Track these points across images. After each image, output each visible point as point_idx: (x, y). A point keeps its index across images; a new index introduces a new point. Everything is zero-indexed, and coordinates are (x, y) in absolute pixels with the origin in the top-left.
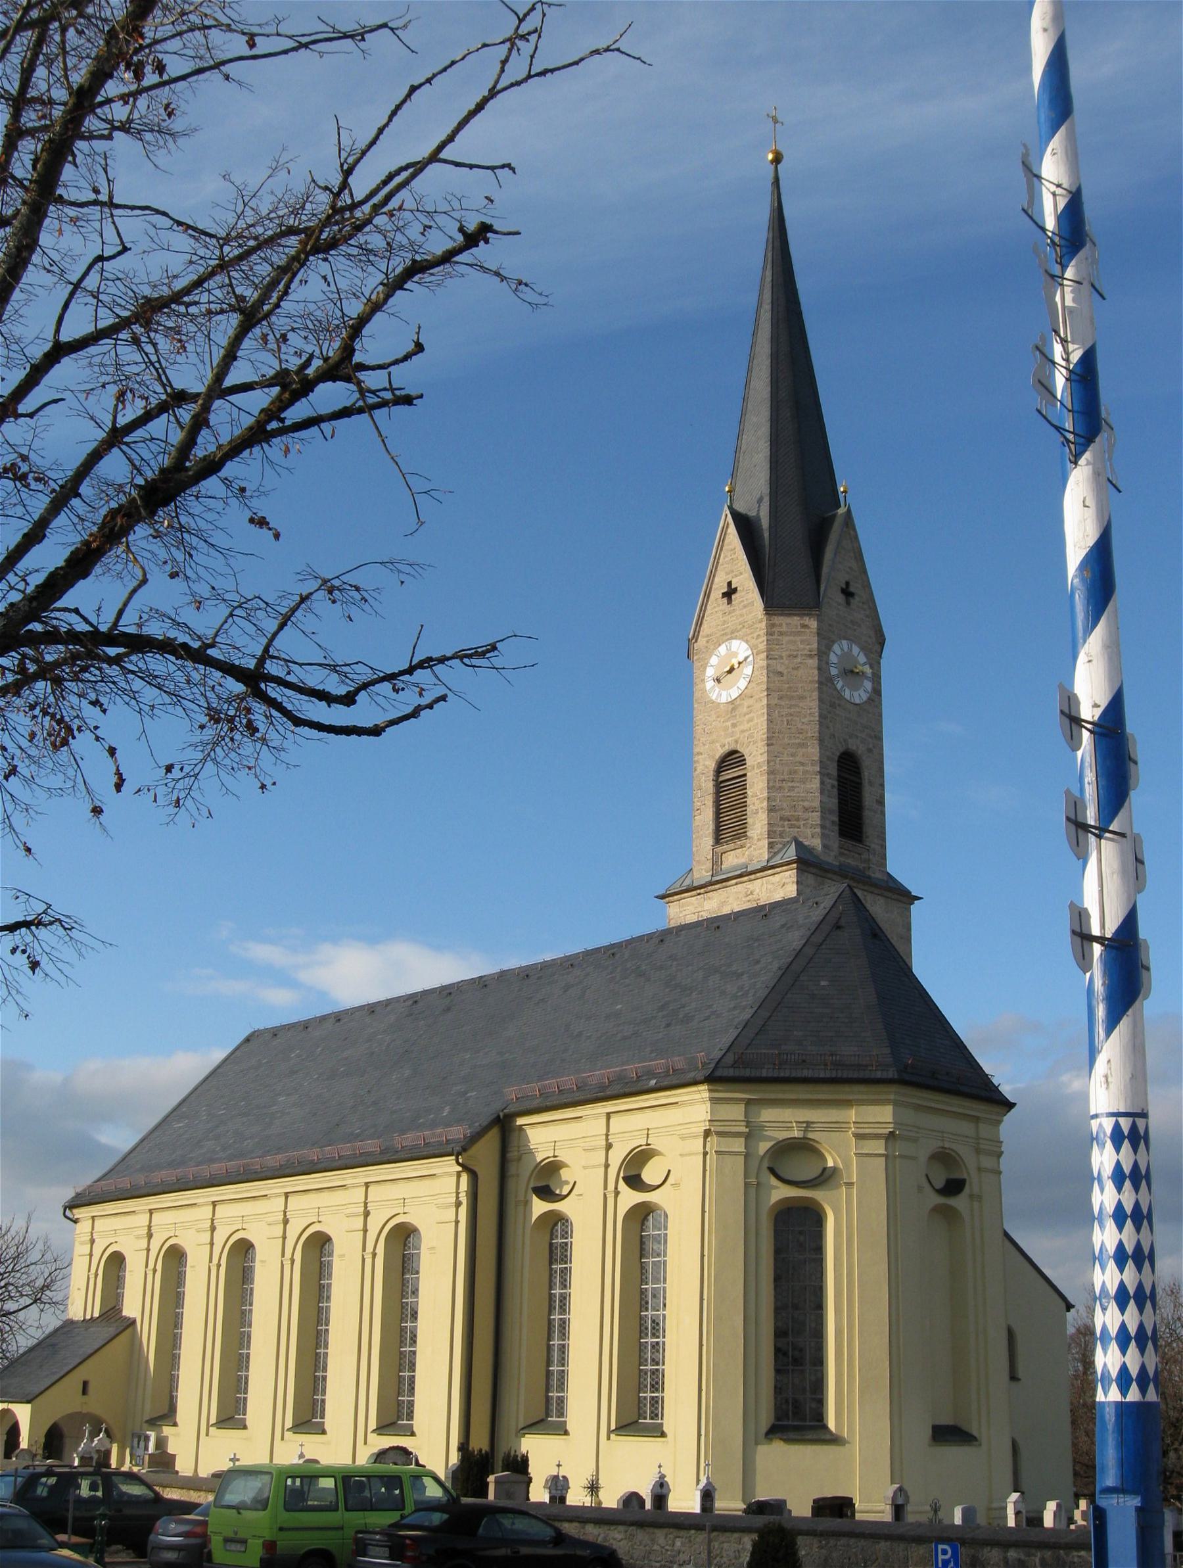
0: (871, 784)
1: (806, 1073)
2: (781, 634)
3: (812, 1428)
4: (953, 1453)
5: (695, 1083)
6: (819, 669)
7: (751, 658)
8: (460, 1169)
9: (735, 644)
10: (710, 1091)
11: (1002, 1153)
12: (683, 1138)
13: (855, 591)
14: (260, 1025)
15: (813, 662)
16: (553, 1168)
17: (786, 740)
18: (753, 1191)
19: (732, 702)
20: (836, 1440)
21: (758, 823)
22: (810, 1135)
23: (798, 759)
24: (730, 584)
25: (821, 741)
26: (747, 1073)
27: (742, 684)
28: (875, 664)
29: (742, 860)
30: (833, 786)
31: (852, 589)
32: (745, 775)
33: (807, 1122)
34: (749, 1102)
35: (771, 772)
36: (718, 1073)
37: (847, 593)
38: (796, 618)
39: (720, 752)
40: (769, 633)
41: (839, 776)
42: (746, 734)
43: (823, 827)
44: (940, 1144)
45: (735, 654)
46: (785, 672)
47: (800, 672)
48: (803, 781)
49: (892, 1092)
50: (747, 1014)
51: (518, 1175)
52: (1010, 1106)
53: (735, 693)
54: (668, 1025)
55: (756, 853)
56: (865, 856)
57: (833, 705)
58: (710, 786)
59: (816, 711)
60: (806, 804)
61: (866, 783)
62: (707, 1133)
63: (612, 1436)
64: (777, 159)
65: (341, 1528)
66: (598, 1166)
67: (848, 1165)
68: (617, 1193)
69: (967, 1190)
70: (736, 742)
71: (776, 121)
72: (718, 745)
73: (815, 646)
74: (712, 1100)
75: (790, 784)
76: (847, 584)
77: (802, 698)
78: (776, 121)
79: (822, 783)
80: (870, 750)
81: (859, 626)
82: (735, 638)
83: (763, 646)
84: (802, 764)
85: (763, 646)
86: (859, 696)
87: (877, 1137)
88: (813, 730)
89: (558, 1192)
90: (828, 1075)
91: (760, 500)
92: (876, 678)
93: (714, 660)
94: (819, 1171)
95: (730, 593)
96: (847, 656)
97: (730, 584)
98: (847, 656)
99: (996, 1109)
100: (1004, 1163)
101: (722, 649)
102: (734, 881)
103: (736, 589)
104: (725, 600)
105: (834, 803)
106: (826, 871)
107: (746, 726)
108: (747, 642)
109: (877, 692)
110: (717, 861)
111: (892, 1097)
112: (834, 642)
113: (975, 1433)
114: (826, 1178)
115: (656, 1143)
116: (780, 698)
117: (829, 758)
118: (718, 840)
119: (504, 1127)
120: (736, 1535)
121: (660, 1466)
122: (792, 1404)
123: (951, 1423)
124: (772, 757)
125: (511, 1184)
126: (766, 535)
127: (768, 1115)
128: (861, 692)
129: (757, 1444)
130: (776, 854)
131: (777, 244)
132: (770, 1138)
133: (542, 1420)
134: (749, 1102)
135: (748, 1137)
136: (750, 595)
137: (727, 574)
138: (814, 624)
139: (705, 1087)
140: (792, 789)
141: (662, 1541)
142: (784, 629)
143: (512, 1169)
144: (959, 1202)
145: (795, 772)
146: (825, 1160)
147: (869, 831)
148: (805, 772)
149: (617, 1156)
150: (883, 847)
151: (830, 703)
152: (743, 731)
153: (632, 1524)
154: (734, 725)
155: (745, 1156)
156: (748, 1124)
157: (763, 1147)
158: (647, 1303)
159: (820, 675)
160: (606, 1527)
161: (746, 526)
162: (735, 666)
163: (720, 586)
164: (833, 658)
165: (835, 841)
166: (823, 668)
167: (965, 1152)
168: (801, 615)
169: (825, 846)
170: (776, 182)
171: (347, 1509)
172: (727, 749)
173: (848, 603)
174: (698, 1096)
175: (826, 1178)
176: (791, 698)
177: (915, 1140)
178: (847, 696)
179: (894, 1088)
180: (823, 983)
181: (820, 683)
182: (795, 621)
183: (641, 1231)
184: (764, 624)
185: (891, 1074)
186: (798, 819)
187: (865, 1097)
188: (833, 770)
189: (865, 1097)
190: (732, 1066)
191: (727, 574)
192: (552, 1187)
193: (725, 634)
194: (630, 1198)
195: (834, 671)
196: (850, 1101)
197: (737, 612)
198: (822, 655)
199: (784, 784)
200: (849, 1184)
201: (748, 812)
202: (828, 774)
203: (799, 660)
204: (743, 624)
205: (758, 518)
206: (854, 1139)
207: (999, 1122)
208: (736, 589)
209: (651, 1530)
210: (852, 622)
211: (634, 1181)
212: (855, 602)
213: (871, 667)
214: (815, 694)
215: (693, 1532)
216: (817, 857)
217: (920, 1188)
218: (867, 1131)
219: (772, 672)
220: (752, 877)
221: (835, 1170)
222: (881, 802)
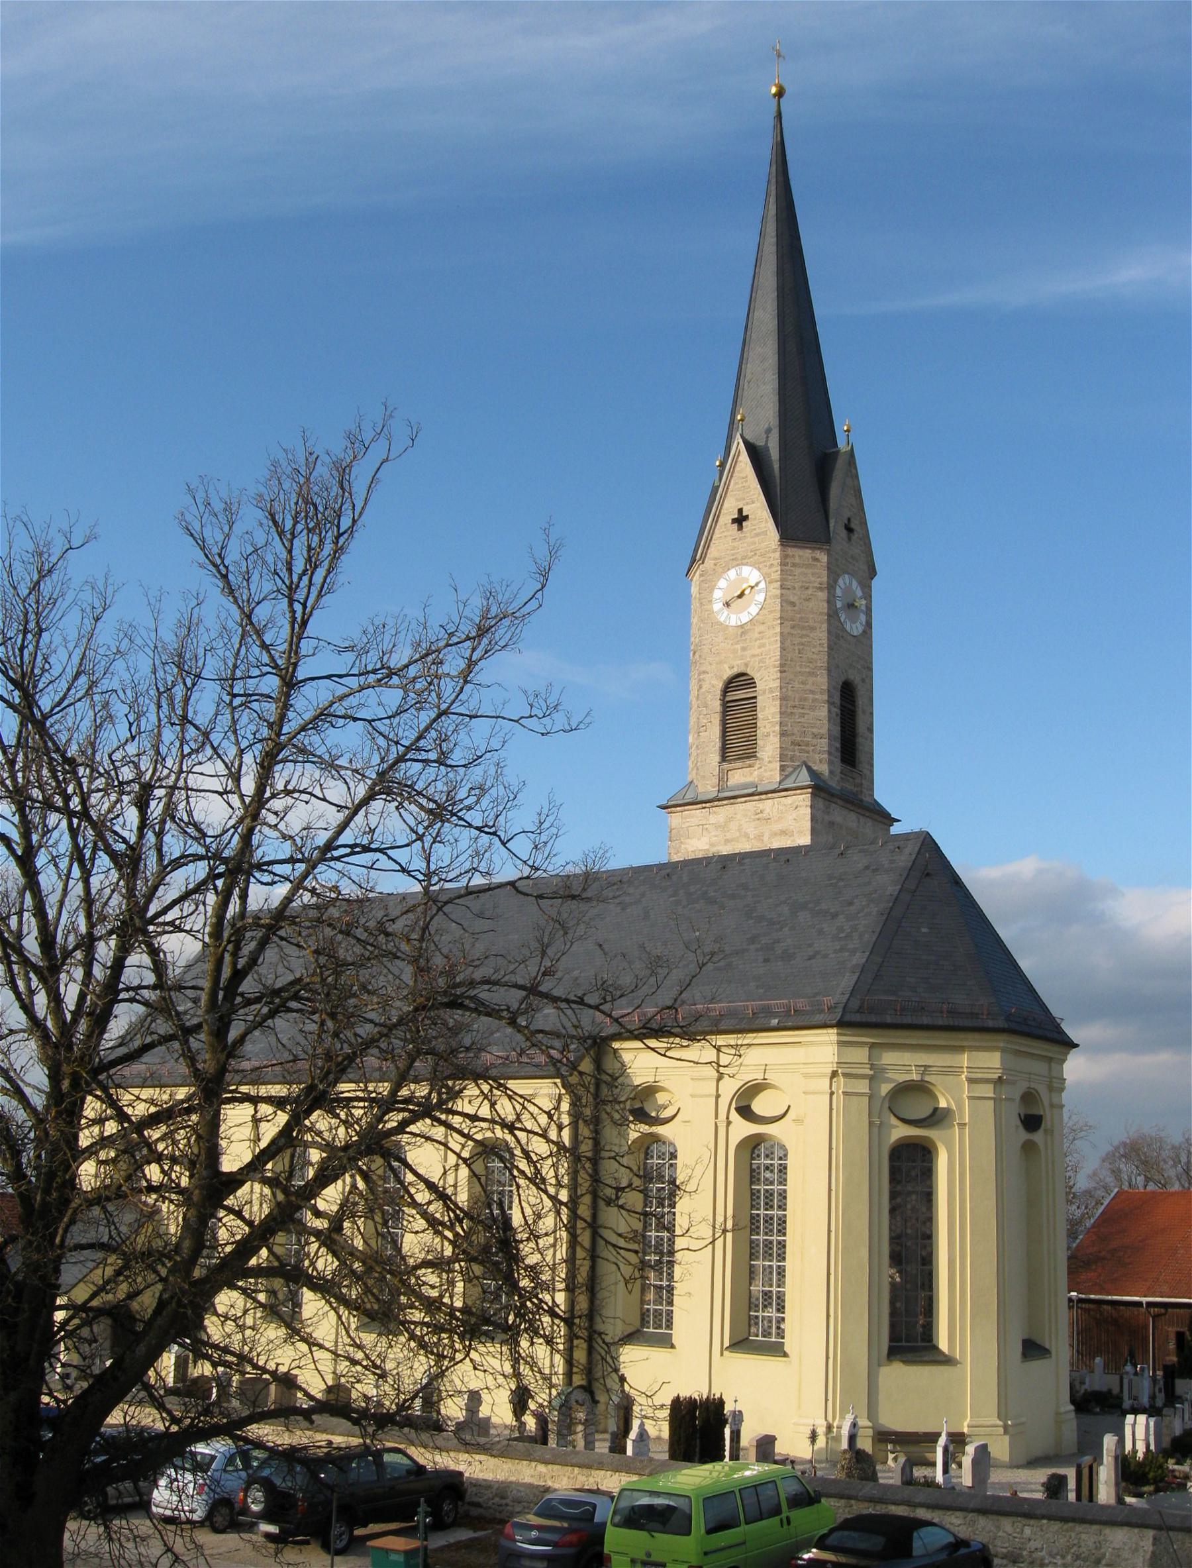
0: (864, 712)
1: (926, 1020)
2: (794, 565)
3: (926, 1349)
5: (831, 1026)
6: (828, 602)
7: (762, 585)
9: (746, 570)
10: (838, 1034)
12: (806, 1076)
13: (855, 528)
15: (823, 595)
16: (650, 1091)
17: (798, 669)
18: (875, 1130)
19: (742, 626)
20: (948, 1361)
21: (769, 745)
22: (927, 1078)
23: (808, 687)
24: (740, 511)
25: (829, 671)
26: (873, 1019)
27: (754, 610)
28: (868, 596)
29: (749, 779)
31: (853, 526)
33: (925, 1066)
34: (872, 1046)
35: (783, 698)
36: (847, 1018)
37: (849, 530)
38: (809, 551)
39: (728, 673)
40: (783, 564)
42: (757, 659)
43: (830, 753)
45: (746, 580)
46: (797, 603)
47: (811, 604)
48: (812, 708)
49: (1001, 1040)
50: (859, 959)
53: (745, 618)
55: (767, 774)
56: (858, 781)
57: (837, 637)
58: (717, 705)
59: (825, 642)
60: (815, 730)
62: (834, 1074)
63: (726, 1353)
64: (780, 94)
65: (744, 1543)
66: (710, 1096)
67: (960, 1107)
68: (729, 1123)
70: (746, 665)
72: (726, 666)
73: (825, 579)
74: (840, 1043)
76: (849, 520)
77: (813, 629)
79: (829, 711)
80: (863, 680)
82: (746, 564)
83: (777, 576)
84: (812, 692)
85: (777, 576)
86: (856, 629)
87: (987, 1081)
88: (822, 660)
89: (653, 1114)
90: (946, 1023)
91: (768, 431)
93: (722, 583)
94: (930, 1111)
95: (740, 520)
96: (848, 590)
97: (740, 511)
98: (848, 590)
101: (732, 574)
103: (747, 516)
104: (735, 526)
105: (837, 730)
106: (833, 795)
107: (758, 651)
108: (759, 569)
109: (869, 624)
110: (722, 778)
111: (1002, 1045)
112: (839, 576)
113: (1047, 1346)
114: (937, 1118)
115: (772, 1078)
116: (793, 627)
117: (834, 688)
118: (724, 758)
119: (599, 1046)
120: (1095, 1527)
122: (907, 1331)
124: (785, 684)
126: (776, 466)
127: (889, 1058)
128: (858, 624)
129: (879, 1365)
130: (787, 776)
131: (781, 178)
132: (890, 1080)
133: (638, 1331)
134: (872, 1046)
135: (872, 1079)
136: (763, 525)
137: (738, 500)
138: (824, 558)
139: (835, 1031)
140: (803, 715)
141: (1009, 1528)
142: (797, 560)
144: (1038, 1137)
145: (805, 699)
146: (936, 1099)
147: (861, 756)
148: (814, 700)
149: (729, 1088)
150: (872, 772)
151: (836, 634)
152: (754, 656)
153: (973, 1511)
154: (744, 649)
155: (870, 1098)
156: (872, 1067)
157: (885, 1089)
158: (758, 1227)
159: (829, 609)
160: (940, 1512)
161: (756, 455)
162: (744, 591)
163: (729, 511)
164: (839, 592)
165: (838, 767)
166: (830, 601)
168: (813, 549)
169: (831, 772)
170: (779, 116)
171: (747, 1523)
172: (735, 671)
173: (849, 539)
174: (827, 1038)
175: (937, 1118)
176: (803, 628)
178: (848, 628)
179: (1004, 1037)
180: (924, 930)
181: (829, 615)
182: (807, 553)
184: (778, 554)
185: (1001, 1023)
186: (807, 745)
187: (989, 1044)
190: (858, 1011)
191: (738, 500)
192: (647, 1109)
194: (742, 1129)
195: (839, 605)
196: (963, 1047)
197: (749, 540)
198: (831, 587)
199: (795, 710)
200: (962, 1125)
201: (759, 736)
202: (833, 703)
203: (810, 592)
204: (755, 552)
205: (766, 448)
206: (965, 1081)
207: (1064, 1061)
208: (747, 516)
209: (995, 1517)
210: (852, 557)
211: (745, 1112)
212: (855, 537)
214: (825, 626)
215: (1045, 1521)
216: (824, 781)
218: (980, 1076)
219: (785, 601)
220: (763, 797)
221: (947, 1112)
222: (871, 730)
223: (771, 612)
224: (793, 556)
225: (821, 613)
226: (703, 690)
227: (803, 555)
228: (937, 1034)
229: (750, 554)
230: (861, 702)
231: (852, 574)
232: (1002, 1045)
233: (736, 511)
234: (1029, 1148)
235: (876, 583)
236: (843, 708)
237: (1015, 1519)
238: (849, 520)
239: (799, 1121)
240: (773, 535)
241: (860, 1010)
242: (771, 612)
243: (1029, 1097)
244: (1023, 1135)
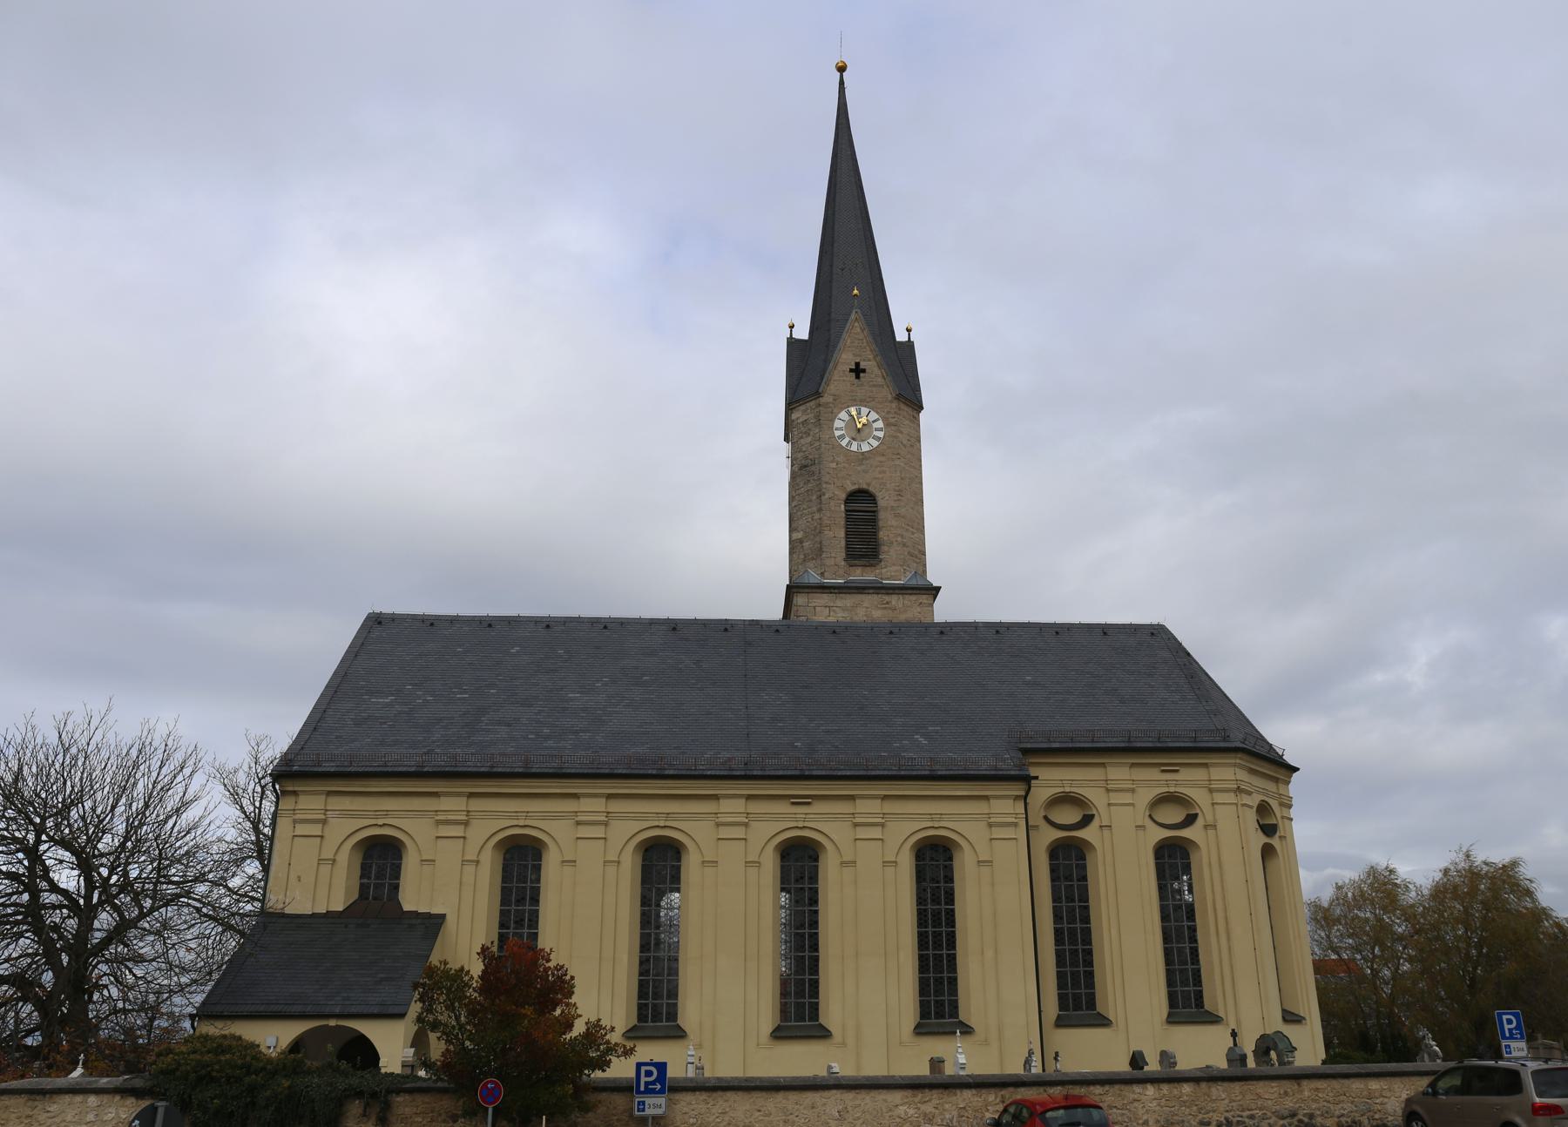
144: (1275, 841)
167: (1274, 804)
243: (1263, 809)
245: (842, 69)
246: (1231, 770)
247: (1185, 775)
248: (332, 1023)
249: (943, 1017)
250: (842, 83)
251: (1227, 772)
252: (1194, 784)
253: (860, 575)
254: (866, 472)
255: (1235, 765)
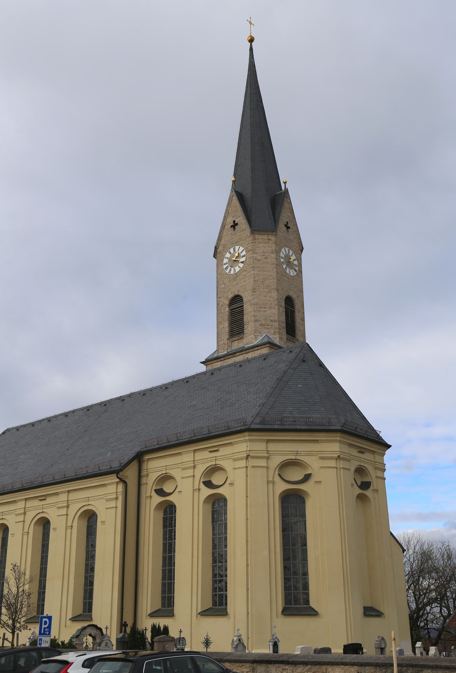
0: (299, 312)
4: (374, 621)
8: (118, 480)
11: (385, 470)
13: (291, 225)
14: (10, 426)
15: (273, 256)
19: (236, 274)
24: (234, 221)
28: (299, 259)
30: (283, 311)
31: (289, 225)
32: (243, 306)
37: (288, 228)
39: (231, 296)
41: (285, 307)
44: (359, 464)
51: (147, 484)
52: (389, 446)
54: (222, 408)
60: (272, 318)
61: (296, 311)
69: (371, 487)
70: (238, 291)
71: (251, 24)
73: (274, 248)
75: (264, 309)
76: (287, 223)
78: (251, 24)
80: (298, 297)
81: (293, 242)
87: (331, 458)
92: (300, 265)
97: (234, 221)
99: (383, 448)
100: (386, 475)
102: (238, 354)
105: (283, 318)
121: (181, 632)
123: (369, 605)
125: (143, 488)
137: (233, 217)
140: (265, 311)
142: (260, 240)
143: (144, 480)
144: (368, 493)
147: (298, 333)
166: (278, 258)
167: (370, 468)
173: (288, 231)
177: (349, 460)
178: (288, 272)
179: (339, 434)
180: (299, 386)
182: (265, 237)
183: (217, 507)
186: (268, 325)
188: (283, 304)
189: (325, 439)
193: (233, 244)
194: (206, 492)
197: (238, 234)
206: (324, 465)
210: (289, 239)
211: (209, 484)
212: (290, 230)
213: (298, 261)
214: (275, 270)
217: (352, 485)
220: (247, 351)
222: (303, 320)
223: (249, 265)
224: (258, 239)
225: (273, 264)
226: (220, 305)
227: (260, 237)
228: (302, 434)
229: (239, 241)
230: (297, 307)
231: (290, 248)
232: (339, 439)
233: (232, 222)
234: (361, 498)
235: (304, 255)
236: (293, 313)
237: (277, 665)
238: (287, 223)
239: (232, 484)
240: (248, 230)
241: (261, 423)
242: (249, 265)
243: (360, 471)
244: (359, 491)
245: (251, 40)
246: (245, 444)
247: (223, 451)
248: (349, 584)
249: (216, 606)
250: (251, 49)
251: (333, 446)
252: (225, 458)
253: (237, 345)
254: (237, 284)
255: (246, 441)
